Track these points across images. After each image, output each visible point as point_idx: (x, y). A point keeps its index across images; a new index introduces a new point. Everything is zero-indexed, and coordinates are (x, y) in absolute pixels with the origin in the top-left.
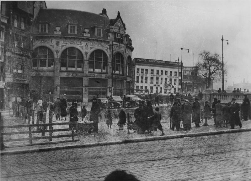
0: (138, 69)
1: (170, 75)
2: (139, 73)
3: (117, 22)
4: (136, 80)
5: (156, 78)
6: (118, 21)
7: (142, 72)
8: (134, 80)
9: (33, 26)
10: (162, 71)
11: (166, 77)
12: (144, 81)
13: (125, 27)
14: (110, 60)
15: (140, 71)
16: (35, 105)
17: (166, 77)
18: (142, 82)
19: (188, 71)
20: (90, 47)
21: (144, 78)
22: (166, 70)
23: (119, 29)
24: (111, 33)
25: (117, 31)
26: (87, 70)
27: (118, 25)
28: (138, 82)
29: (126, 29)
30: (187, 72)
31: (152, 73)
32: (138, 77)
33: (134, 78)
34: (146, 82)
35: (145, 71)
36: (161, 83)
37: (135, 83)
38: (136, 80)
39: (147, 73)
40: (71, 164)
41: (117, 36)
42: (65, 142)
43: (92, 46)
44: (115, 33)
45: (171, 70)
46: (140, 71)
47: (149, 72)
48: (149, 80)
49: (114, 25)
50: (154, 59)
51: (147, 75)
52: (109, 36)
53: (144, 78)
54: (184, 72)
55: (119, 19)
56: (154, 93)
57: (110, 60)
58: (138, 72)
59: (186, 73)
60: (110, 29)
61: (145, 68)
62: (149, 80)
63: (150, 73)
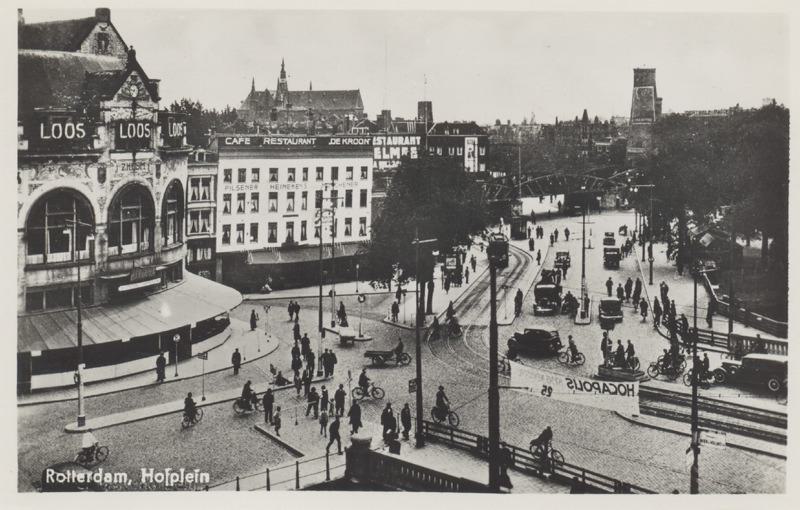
0: (228, 172)
3: (126, 85)
4: (221, 205)
6: (129, 79)
7: (242, 179)
10: (306, 170)
12: (249, 207)
13: (157, 94)
14: (101, 216)
15: (235, 176)
17: (319, 186)
19: (395, 146)
20: (31, 186)
21: (248, 198)
22: (272, 221)
23: (134, 106)
24: (104, 124)
25: (126, 114)
27: (130, 95)
29: (160, 99)
30: (392, 149)
32: (227, 197)
34: (255, 210)
36: (304, 208)
38: (221, 205)
41: (125, 133)
42: (461, 438)
43: (37, 179)
44: (114, 125)
46: (235, 176)
47: (265, 175)
48: (265, 202)
49: (115, 98)
51: (256, 187)
52: (98, 138)
53: (248, 198)
54: (384, 149)
55: (133, 73)
56: (283, 244)
57: (101, 216)
58: (228, 179)
59: (388, 152)
60: (101, 113)
61: (249, 164)
62: (265, 202)
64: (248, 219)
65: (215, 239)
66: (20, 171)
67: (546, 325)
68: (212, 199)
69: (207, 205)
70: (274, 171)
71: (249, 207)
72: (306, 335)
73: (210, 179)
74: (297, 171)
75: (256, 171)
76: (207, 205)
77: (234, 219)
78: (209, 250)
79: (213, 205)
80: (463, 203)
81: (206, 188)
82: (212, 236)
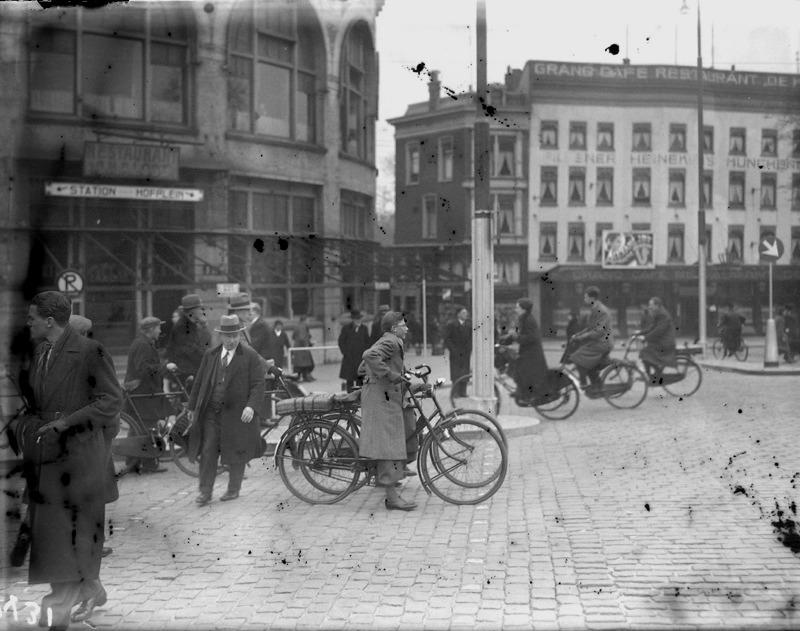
1: (766, 149)
2: (683, 149)
4: (536, 188)
5: (665, 176)
8: (526, 191)
9: (773, 617)
11: (640, 160)
12: (591, 196)
16: (253, 208)
17: (640, 160)
18: (577, 198)
26: (289, 285)
28: (549, 199)
31: (739, 151)
33: (526, 177)
35: (593, 139)
37: (534, 206)
38: (536, 188)
39: (607, 147)
40: (189, 565)
45: (736, 119)
47: (623, 138)
50: (670, 62)
63: (727, 150)
64: (591, 161)
65: (525, 249)
66: (368, 17)
67: (302, 286)
68: (519, 172)
69: (511, 184)
70: (642, 129)
71: (591, 196)
72: (110, 551)
73: (514, 197)
74: (749, 134)
75: (606, 128)
76: (511, 184)
77: (565, 159)
78: (516, 268)
79: (521, 185)
80: (273, 395)
81: (509, 155)
82: (520, 242)
